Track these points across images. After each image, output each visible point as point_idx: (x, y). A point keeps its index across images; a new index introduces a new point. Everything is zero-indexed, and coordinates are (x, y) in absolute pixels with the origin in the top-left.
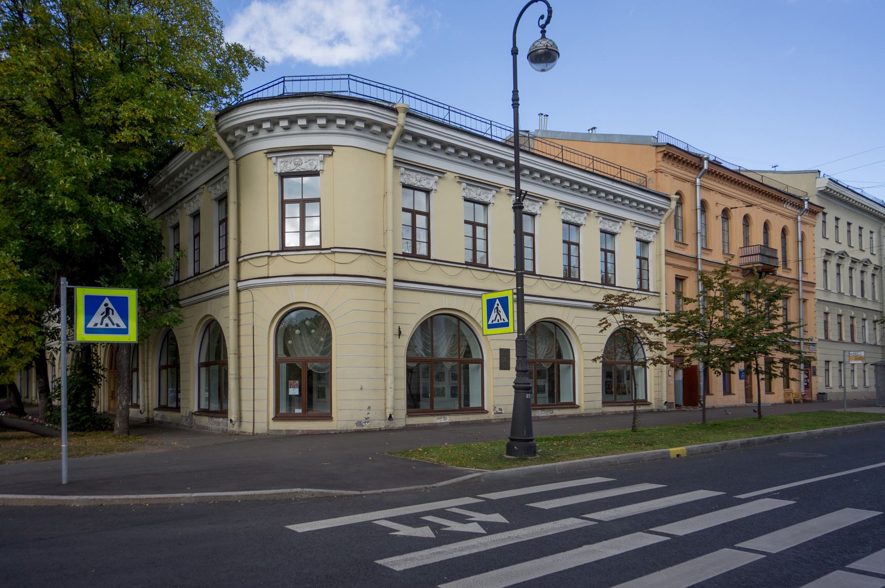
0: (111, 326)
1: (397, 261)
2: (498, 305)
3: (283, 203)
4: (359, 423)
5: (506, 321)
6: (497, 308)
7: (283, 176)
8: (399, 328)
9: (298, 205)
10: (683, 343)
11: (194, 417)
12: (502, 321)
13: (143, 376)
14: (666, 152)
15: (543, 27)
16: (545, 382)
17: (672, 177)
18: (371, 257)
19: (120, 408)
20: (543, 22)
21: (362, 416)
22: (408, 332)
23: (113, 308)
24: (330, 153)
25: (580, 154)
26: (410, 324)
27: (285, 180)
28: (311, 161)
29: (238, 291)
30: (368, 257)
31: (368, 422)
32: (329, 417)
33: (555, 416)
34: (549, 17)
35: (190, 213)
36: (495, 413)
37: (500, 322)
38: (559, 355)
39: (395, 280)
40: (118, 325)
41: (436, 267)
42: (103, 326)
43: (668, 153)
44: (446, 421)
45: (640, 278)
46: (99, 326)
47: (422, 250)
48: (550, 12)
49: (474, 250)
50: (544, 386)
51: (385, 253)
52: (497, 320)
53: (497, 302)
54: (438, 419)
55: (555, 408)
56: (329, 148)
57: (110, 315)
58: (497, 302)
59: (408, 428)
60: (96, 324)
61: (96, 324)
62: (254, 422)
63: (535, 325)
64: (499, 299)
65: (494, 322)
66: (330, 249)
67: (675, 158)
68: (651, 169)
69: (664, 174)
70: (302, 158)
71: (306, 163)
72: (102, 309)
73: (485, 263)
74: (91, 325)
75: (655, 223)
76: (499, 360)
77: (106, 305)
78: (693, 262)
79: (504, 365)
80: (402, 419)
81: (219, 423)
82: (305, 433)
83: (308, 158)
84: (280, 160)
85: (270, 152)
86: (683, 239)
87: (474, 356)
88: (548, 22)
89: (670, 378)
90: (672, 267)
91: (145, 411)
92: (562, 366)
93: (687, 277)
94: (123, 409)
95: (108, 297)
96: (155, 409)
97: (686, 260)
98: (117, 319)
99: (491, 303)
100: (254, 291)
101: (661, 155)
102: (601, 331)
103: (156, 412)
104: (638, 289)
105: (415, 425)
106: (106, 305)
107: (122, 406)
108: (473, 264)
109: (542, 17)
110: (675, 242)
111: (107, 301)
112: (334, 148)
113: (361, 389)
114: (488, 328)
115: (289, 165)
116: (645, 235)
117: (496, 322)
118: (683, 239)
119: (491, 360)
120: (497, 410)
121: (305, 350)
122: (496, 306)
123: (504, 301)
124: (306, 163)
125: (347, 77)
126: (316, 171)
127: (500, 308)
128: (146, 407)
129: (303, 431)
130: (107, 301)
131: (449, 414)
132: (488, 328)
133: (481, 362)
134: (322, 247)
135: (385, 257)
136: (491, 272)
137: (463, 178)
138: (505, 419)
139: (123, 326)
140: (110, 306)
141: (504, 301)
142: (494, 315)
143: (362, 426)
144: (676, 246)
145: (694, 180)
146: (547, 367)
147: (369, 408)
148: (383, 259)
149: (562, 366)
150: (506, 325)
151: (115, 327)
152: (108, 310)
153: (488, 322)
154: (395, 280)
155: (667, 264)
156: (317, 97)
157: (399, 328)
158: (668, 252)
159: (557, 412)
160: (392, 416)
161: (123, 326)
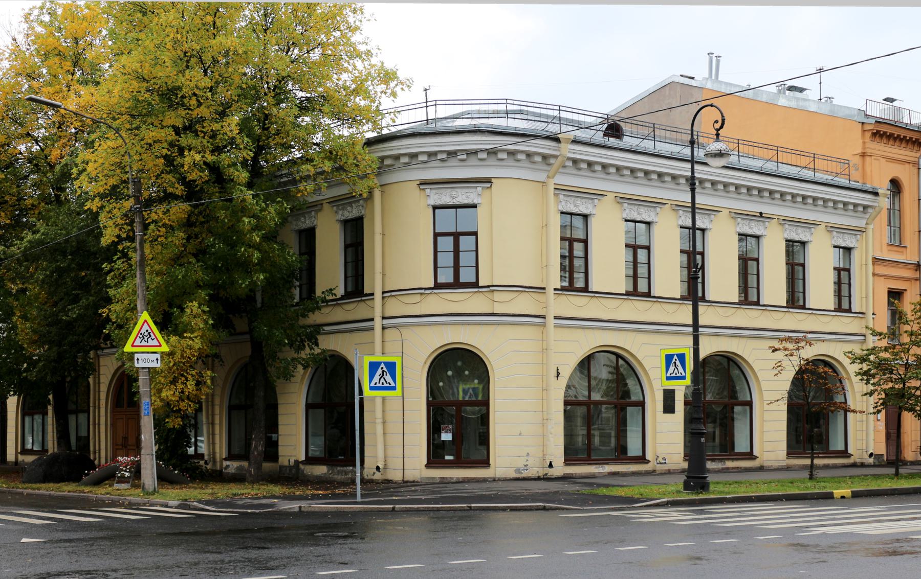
0: (385, 384)
1: (557, 296)
2: (676, 360)
3: (436, 235)
4: (518, 471)
5: (684, 374)
6: (675, 363)
7: (435, 208)
8: (558, 370)
9: (451, 238)
10: (873, 384)
11: (302, 466)
12: (680, 375)
13: (207, 418)
14: (875, 131)
15: (718, 130)
16: (714, 428)
17: (885, 160)
18: (530, 293)
19: (256, 453)
20: (718, 126)
21: (520, 464)
22: (566, 372)
23: (386, 370)
24: (488, 185)
25: (761, 146)
26: (569, 364)
27: (436, 210)
28: (468, 194)
29: (383, 328)
30: (527, 294)
31: (527, 470)
32: (485, 463)
33: (728, 468)
34: (723, 121)
35: (297, 228)
36: (657, 463)
37: (678, 375)
38: (733, 394)
39: (556, 318)
40: (390, 384)
41: (595, 299)
42: (381, 385)
43: (878, 132)
44: (605, 471)
45: (839, 294)
46: (378, 385)
47: (845, 306)
48: (723, 121)
49: (635, 277)
50: (714, 432)
51: (544, 289)
52: (675, 373)
53: (675, 357)
54: (596, 468)
55: (728, 459)
56: (488, 181)
57: (385, 376)
58: (675, 357)
59: (565, 478)
60: (376, 384)
61: (376, 384)
62: (404, 469)
63: (704, 360)
64: (677, 355)
65: (672, 375)
66: (488, 287)
67: (895, 139)
68: (855, 153)
69: (873, 157)
70: (459, 190)
71: (462, 196)
72: (379, 371)
73: (755, 300)
74: (373, 384)
75: (862, 223)
76: (662, 402)
77: (382, 368)
78: (913, 270)
79: (669, 408)
80: (560, 469)
81: (346, 473)
82: (461, 480)
83: (466, 190)
84: (434, 191)
85: (423, 183)
86: (900, 241)
87: (633, 398)
88: (722, 127)
89: (879, 423)
90: (882, 279)
91: (210, 461)
92: (737, 409)
93: (906, 290)
94: (258, 454)
95: (384, 362)
96: (226, 459)
97: (904, 268)
98: (388, 378)
99: (669, 358)
100: (403, 330)
101: (868, 134)
102: (776, 375)
103: (225, 463)
104: (835, 310)
105: (572, 474)
106: (382, 368)
107: (258, 451)
108: (634, 293)
109: (716, 122)
110: (888, 245)
111: (382, 365)
112: (493, 180)
113: (520, 434)
114: (667, 380)
115: (444, 197)
116: (848, 242)
117: (674, 375)
118: (900, 241)
119: (654, 403)
120: (660, 460)
121: (462, 391)
122: (674, 361)
123: (682, 357)
124: (462, 196)
125: (505, 101)
126: (474, 204)
127: (678, 363)
128: (211, 456)
129: (458, 478)
130: (382, 365)
131: (607, 464)
132: (667, 380)
133: (642, 404)
134: (480, 285)
135: (545, 293)
136: (655, 301)
137: (623, 199)
138: (669, 470)
139: (393, 384)
140: (385, 369)
141: (682, 357)
142: (672, 368)
143: (521, 473)
144: (889, 250)
145: (917, 160)
146: (719, 409)
147: (528, 454)
148: (541, 295)
149: (737, 409)
150: (684, 378)
151: (388, 385)
152: (383, 372)
153: (666, 373)
154: (556, 318)
155: (874, 275)
156: (480, 133)
157: (558, 370)
158: (876, 260)
159: (730, 464)
160: (553, 463)
161: (393, 384)
